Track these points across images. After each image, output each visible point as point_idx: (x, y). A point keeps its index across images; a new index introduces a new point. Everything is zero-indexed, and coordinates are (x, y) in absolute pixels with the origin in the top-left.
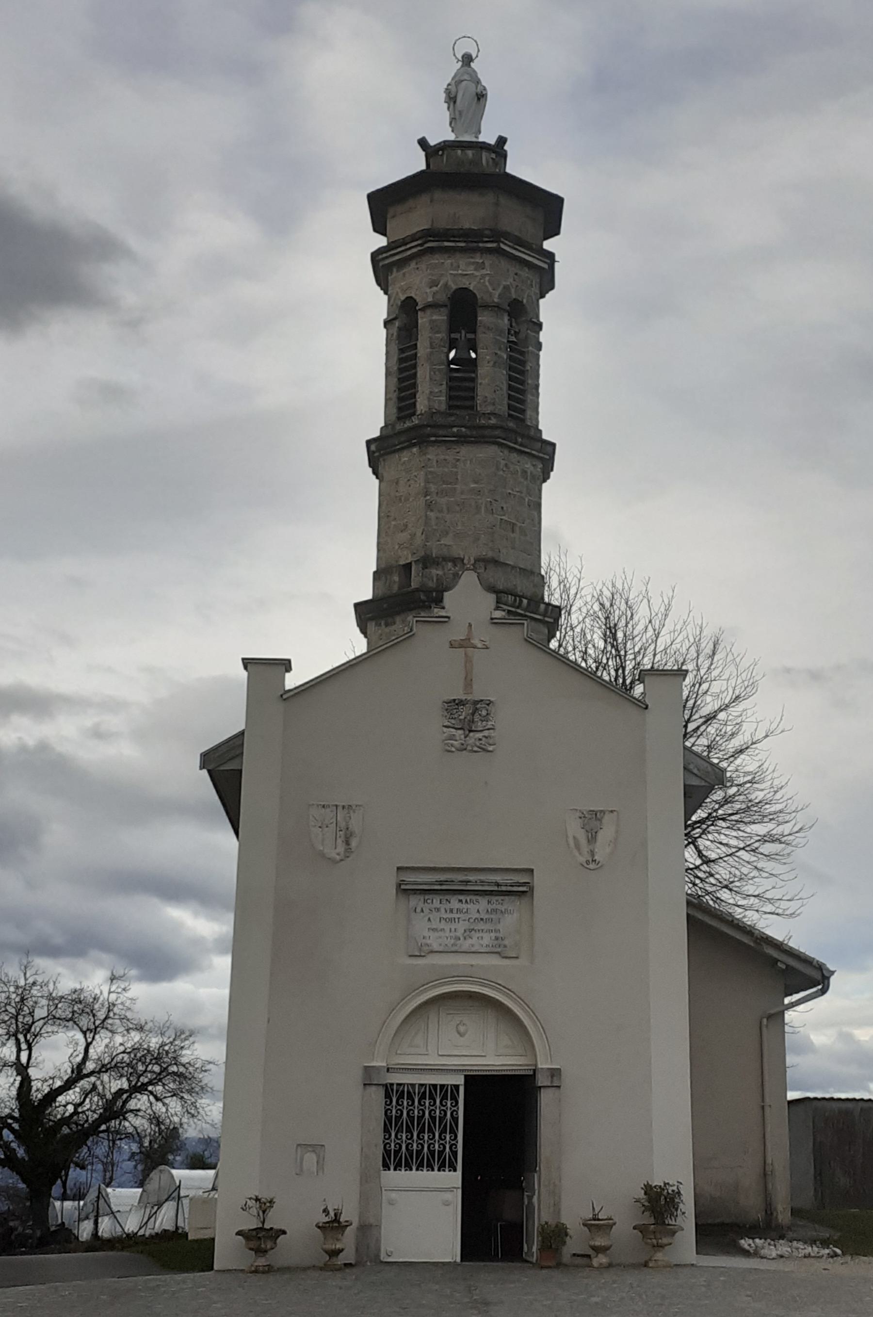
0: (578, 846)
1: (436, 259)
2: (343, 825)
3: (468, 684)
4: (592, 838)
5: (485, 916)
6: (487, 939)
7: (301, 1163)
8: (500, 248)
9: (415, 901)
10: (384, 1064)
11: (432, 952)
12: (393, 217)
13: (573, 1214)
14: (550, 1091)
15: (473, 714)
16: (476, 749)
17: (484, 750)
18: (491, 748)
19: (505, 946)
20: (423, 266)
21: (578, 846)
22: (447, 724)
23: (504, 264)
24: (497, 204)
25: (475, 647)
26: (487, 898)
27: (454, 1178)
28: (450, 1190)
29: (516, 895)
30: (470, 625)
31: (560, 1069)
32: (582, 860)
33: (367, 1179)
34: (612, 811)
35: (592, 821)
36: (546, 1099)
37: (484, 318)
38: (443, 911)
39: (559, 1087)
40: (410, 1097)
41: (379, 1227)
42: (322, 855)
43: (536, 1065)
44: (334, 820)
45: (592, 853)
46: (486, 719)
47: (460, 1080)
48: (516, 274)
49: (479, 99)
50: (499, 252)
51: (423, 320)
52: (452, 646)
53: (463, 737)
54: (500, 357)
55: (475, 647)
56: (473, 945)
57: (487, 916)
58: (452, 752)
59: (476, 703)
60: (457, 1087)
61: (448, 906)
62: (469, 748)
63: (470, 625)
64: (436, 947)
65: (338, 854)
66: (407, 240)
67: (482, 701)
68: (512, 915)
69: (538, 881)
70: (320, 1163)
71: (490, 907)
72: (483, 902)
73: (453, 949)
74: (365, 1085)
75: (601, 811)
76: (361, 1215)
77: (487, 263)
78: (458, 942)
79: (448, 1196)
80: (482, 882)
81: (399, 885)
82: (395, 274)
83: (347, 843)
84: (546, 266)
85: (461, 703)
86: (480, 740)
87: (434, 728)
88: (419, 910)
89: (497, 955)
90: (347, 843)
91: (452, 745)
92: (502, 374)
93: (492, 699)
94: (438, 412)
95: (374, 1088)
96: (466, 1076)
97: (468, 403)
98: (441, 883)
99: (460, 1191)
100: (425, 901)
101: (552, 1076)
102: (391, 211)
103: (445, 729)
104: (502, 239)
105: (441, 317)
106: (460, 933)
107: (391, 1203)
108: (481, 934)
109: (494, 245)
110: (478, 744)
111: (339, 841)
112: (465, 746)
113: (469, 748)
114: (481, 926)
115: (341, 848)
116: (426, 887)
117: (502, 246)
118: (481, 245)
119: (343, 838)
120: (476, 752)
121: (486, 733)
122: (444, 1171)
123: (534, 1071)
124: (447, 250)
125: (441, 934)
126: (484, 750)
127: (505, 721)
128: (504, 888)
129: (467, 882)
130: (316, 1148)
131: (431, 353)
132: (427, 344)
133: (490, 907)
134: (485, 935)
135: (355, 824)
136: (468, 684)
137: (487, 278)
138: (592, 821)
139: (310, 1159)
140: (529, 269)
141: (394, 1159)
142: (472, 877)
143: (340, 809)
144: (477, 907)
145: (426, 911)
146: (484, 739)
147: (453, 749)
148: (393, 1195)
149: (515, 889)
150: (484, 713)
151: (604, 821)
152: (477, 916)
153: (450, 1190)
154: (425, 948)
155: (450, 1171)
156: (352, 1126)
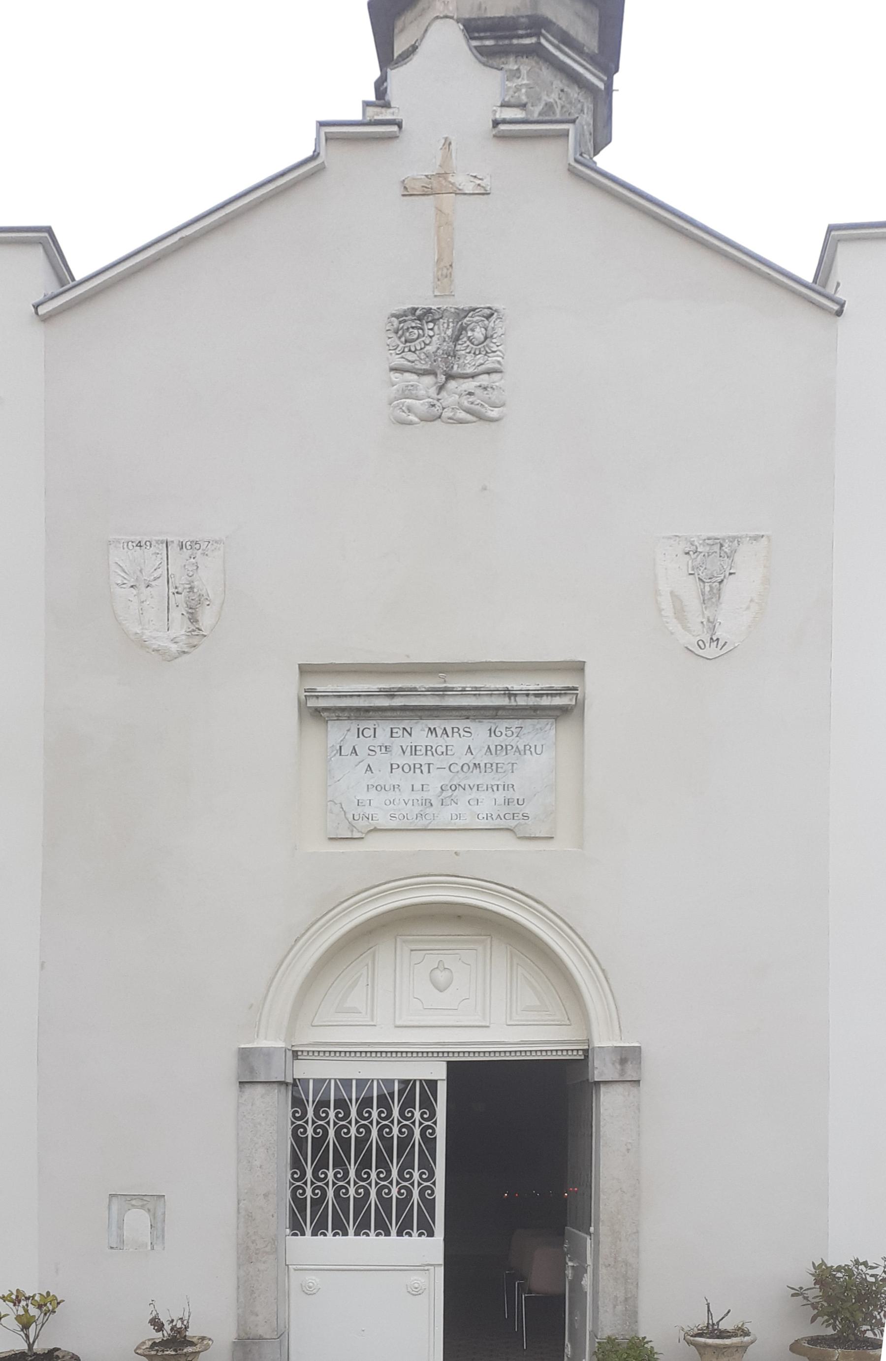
0: (680, 613)
2: (180, 580)
3: (445, 271)
4: (712, 590)
5: (482, 759)
6: (488, 804)
7: (120, 1227)
8: (540, 43)
9: (339, 732)
10: (281, 1044)
11: (375, 830)
12: (402, 31)
13: (662, 1320)
14: (620, 1089)
15: (456, 339)
16: (462, 415)
17: (481, 418)
18: (494, 413)
19: (526, 817)
21: (680, 613)
22: (397, 361)
23: (546, 73)
25: (459, 193)
26: (486, 725)
27: (429, 1250)
28: (423, 1268)
29: (549, 717)
30: (448, 143)
31: (640, 1047)
32: (691, 640)
33: (248, 1254)
34: (756, 538)
35: (713, 562)
36: (611, 1109)
38: (396, 750)
39: (638, 1082)
40: (342, 1104)
41: (282, 1336)
42: (142, 643)
43: (588, 1041)
44: (162, 571)
45: (712, 625)
46: (485, 344)
47: (438, 1072)
48: (562, 91)
50: (537, 52)
52: (407, 193)
53: (433, 391)
55: (459, 193)
56: (459, 816)
57: (487, 759)
58: (411, 423)
59: (461, 314)
60: (433, 1084)
61: (406, 742)
62: (447, 414)
63: (448, 143)
64: (383, 821)
65: (174, 641)
67: (474, 310)
68: (539, 753)
69: (595, 688)
70: (157, 1228)
71: (494, 741)
72: (480, 731)
73: (421, 823)
74: (240, 1082)
75: (734, 538)
76: (241, 1323)
77: (524, 71)
78: (429, 810)
79: (418, 1279)
80: (477, 692)
81: (302, 706)
83: (193, 618)
84: (601, 86)
85: (425, 316)
86: (470, 394)
87: (370, 372)
89: (507, 836)
90: (193, 618)
91: (410, 409)
93: (495, 306)
95: (260, 1089)
98: (391, 694)
99: (440, 1272)
100: (360, 733)
101: (623, 1061)
102: (399, 24)
103: (395, 376)
104: (543, 31)
106: (432, 793)
107: (308, 1292)
108: (474, 794)
110: (466, 404)
111: (176, 614)
112: (436, 411)
113: (447, 414)
114: (476, 778)
115: (180, 627)
116: (357, 703)
117: (543, 41)
118: (515, 41)
119: (183, 609)
120: (461, 422)
121: (484, 380)
122: (410, 1235)
123: (586, 1052)
125: (391, 795)
126: (481, 418)
127: (527, 354)
128: (521, 701)
129: (443, 692)
130: (151, 1203)
133: (494, 741)
134: (482, 796)
135: (208, 580)
136: (445, 271)
137: (524, 91)
138: (713, 562)
139: (137, 1221)
140: (579, 87)
141: (310, 1213)
142: (457, 683)
143: (174, 550)
144: (466, 741)
145: (362, 751)
146: (479, 392)
147: (414, 419)
148: (312, 1279)
149: (545, 701)
150: (479, 334)
151: (737, 557)
153: (423, 1268)
154: (362, 824)
155: (420, 1235)
156: (230, 1157)
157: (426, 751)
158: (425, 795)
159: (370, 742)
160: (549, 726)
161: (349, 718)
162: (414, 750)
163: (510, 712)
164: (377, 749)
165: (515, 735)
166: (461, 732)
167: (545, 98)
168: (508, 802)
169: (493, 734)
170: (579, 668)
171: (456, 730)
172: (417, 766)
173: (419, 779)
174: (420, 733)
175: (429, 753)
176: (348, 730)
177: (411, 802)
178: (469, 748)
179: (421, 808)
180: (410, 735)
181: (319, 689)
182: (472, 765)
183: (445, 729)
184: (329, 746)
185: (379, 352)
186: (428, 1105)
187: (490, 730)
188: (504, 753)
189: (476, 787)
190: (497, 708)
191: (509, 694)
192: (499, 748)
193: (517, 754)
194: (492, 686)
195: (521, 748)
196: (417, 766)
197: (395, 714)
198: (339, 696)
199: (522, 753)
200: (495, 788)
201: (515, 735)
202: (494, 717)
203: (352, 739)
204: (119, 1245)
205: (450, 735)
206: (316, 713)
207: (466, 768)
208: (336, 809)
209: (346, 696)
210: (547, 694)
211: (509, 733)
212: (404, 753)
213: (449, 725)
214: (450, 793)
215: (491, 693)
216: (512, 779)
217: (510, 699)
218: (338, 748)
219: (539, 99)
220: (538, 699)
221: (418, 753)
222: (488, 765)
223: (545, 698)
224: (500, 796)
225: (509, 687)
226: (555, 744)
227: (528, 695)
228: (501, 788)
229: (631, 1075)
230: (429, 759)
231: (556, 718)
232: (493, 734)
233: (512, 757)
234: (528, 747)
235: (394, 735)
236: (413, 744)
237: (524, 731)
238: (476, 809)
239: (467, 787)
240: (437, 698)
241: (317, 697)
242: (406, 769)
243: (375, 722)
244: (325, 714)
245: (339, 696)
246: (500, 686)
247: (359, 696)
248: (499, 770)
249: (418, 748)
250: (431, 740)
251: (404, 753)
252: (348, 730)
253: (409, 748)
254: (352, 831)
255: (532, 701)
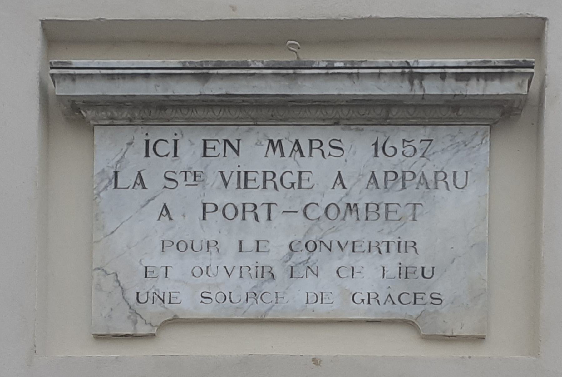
5: (361, 195)
6: (371, 276)
9: (114, 148)
11: (175, 321)
19: (436, 299)
56: (320, 298)
61: (230, 164)
64: (188, 304)
71: (382, 164)
73: (254, 309)
78: (269, 287)
98: (203, 74)
100: (150, 149)
106: (275, 255)
108: (347, 259)
114: (350, 230)
125: (203, 259)
128: (433, 88)
133: (382, 164)
145: (154, 182)
149: (475, 88)
154: (154, 312)
157: (265, 181)
158: (263, 259)
159: (168, 164)
160: (477, 140)
161: (131, 122)
162: (244, 179)
163: (411, 110)
164: (180, 178)
165: (419, 154)
166: (326, 148)
169: (380, 152)
170: (532, 32)
171: (316, 144)
172: (249, 208)
173: (252, 231)
174: (254, 151)
175: (270, 184)
176: (130, 144)
177: (237, 272)
178: (339, 175)
179: (254, 282)
180: (237, 152)
181: (77, 62)
182: (343, 207)
183: (297, 142)
184: (97, 170)
187: (376, 144)
188: (400, 185)
189: (350, 247)
191: (411, 74)
192: (391, 176)
193: (422, 188)
194: (381, 61)
195: (430, 176)
196: (249, 208)
197: (210, 114)
198: (112, 77)
199: (431, 186)
200: (383, 248)
201: (419, 154)
202: (385, 121)
203: (136, 160)
204: (367, 188)
205: (306, 152)
206: (74, 113)
207: (332, 212)
208: (109, 283)
209: (123, 76)
210: (478, 75)
211: (409, 150)
212: (226, 184)
214: (304, 255)
215: (379, 73)
216: (415, 232)
217: (412, 84)
218: (112, 174)
220: (462, 84)
221: (250, 185)
222: (372, 208)
223: (473, 82)
224: (392, 262)
225: (412, 62)
226: (489, 170)
227: (443, 76)
228: (393, 248)
230: (270, 195)
231: (493, 125)
232: (380, 152)
233: (413, 192)
234: (441, 176)
235: (209, 152)
236: (242, 169)
237: (436, 147)
238: (349, 285)
239: (335, 244)
240: (285, 82)
241: (73, 77)
242: (230, 212)
243: (176, 129)
244: (88, 114)
245: (112, 77)
246: (396, 60)
247: (147, 75)
248: (391, 216)
249: (250, 176)
250: (273, 162)
251: (226, 184)
252: (130, 144)
253: (235, 175)
254: (135, 323)
255: (451, 88)
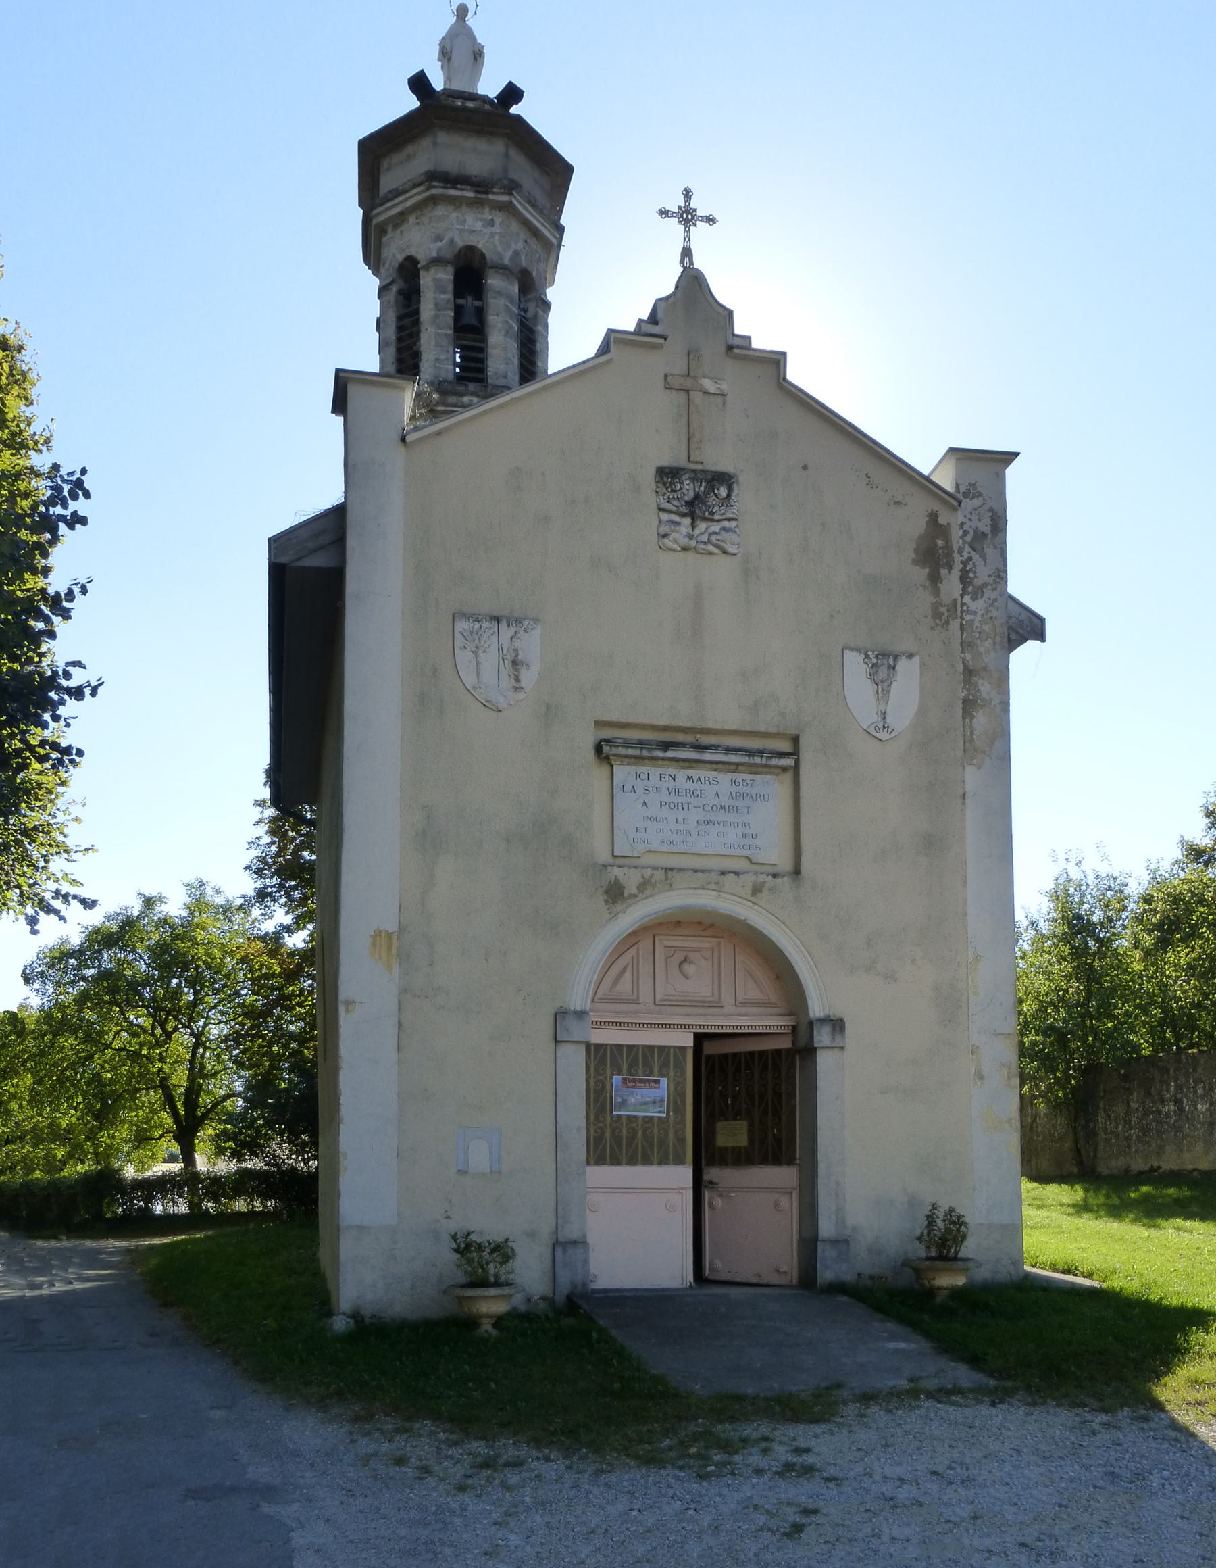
1: (440, 211)
12: (388, 169)
14: (829, 1053)
16: (711, 548)
17: (725, 552)
19: (758, 848)
20: (425, 220)
23: (514, 226)
24: (507, 155)
37: (494, 282)
39: (842, 1048)
47: (689, 1041)
49: (475, 59)
50: (507, 208)
51: (427, 280)
54: (511, 327)
56: (710, 845)
57: (732, 802)
60: (683, 1049)
61: (672, 785)
66: (407, 187)
71: (734, 789)
73: (682, 849)
78: (690, 839)
82: (390, 234)
84: (555, 241)
88: (628, 788)
92: (513, 347)
94: (445, 381)
96: (696, 1035)
97: (478, 365)
102: (385, 164)
105: (446, 275)
108: (722, 829)
109: (505, 198)
114: (721, 816)
121: (726, 524)
124: (451, 201)
126: (725, 552)
131: (436, 316)
132: (431, 306)
133: (734, 789)
152: (716, 801)
161: (629, 764)
162: (677, 792)
167: (513, 246)
168: (745, 836)
173: (681, 815)
185: (649, 495)
186: (680, 1066)
190: (738, 764)
213: (702, 774)
219: (509, 246)
229: (838, 1043)
230: (688, 799)
250: (690, 786)
